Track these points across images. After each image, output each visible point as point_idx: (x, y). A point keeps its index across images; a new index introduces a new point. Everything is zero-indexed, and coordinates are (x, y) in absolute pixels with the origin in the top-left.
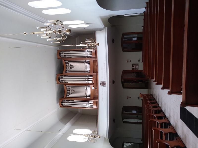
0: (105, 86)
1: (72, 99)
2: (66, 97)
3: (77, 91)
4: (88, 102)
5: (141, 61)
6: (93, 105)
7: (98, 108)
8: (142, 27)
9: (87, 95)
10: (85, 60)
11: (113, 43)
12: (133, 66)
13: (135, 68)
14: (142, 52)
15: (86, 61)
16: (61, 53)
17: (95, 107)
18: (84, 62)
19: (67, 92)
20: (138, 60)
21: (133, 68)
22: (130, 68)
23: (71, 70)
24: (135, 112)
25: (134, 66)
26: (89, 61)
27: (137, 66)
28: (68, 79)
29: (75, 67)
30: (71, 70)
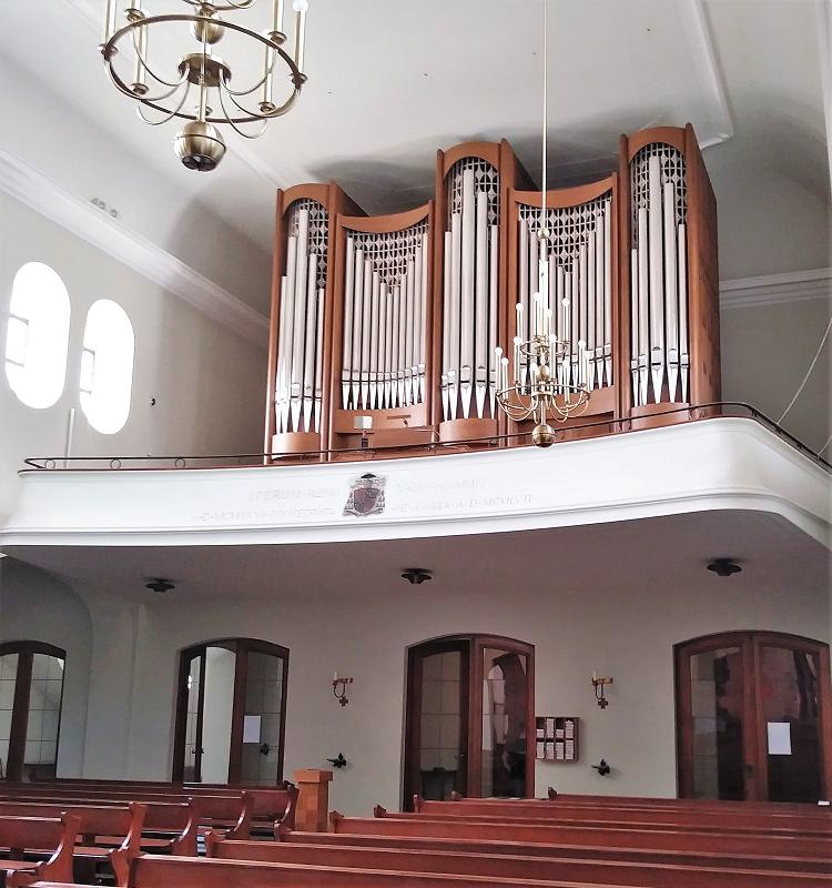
0: (347, 512)
1: (331, 276)
2: (348, 231)
3: (386, 307)
4: (308, 393)
6: (290, 429)
7: (271, 462)
12: (559, 723)
16: (674, 159)
17: (281, 444)
18: (600, 342)
19: (385, 236)
20: (608, 764)
22: (547, 701)
23: (359, 252)
25: (560, 733)
26: (605, 384)
27: (560, 757)
28: (470, 198)
29: (567, 274)
30: (359, 252)
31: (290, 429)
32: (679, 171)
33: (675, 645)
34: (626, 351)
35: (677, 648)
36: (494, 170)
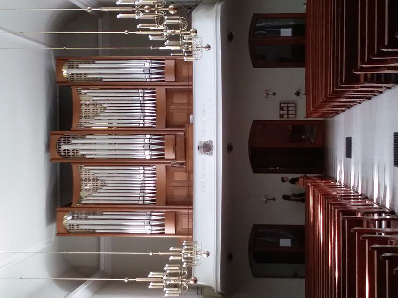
0: (211, 154)
5: (303, 92)
6: (162, 150)
8: (304, 4)
9: (144, 196)
10: (143, 89)
11: (231, 42)
12: (281, 109)
13: (288, 114)
14: (304, 69)
15: (144, 97)
16: (62, 139)
21: (282, 112)
22: (271, 113)
24: (285, 243)
27: (294, 109)
31: (162, 150)
32: (68, 138)
33: (254, 67)
34: (143, 83)
35: (254, 67)
36: (61, 138)
